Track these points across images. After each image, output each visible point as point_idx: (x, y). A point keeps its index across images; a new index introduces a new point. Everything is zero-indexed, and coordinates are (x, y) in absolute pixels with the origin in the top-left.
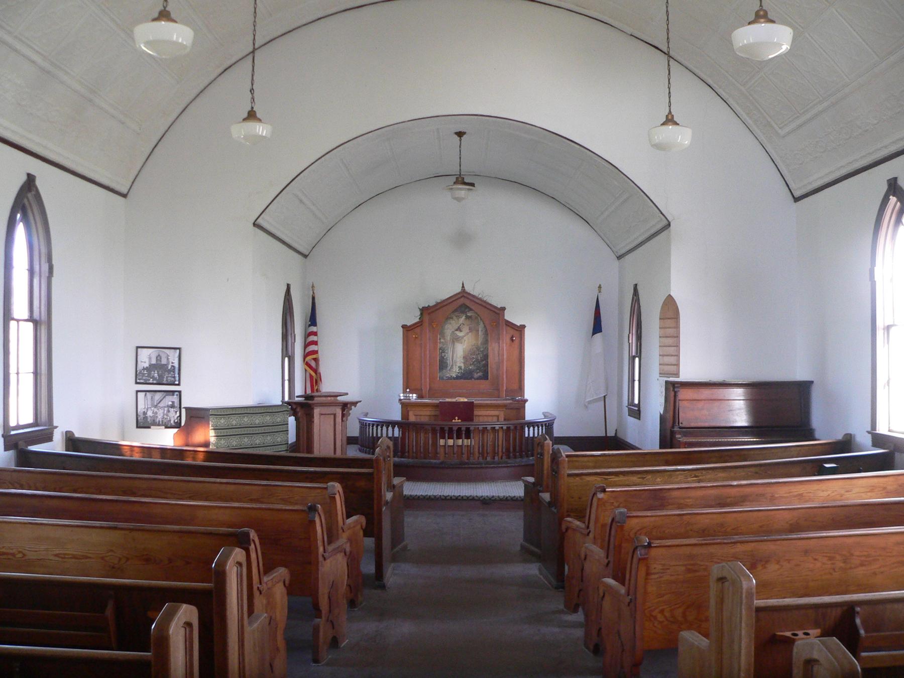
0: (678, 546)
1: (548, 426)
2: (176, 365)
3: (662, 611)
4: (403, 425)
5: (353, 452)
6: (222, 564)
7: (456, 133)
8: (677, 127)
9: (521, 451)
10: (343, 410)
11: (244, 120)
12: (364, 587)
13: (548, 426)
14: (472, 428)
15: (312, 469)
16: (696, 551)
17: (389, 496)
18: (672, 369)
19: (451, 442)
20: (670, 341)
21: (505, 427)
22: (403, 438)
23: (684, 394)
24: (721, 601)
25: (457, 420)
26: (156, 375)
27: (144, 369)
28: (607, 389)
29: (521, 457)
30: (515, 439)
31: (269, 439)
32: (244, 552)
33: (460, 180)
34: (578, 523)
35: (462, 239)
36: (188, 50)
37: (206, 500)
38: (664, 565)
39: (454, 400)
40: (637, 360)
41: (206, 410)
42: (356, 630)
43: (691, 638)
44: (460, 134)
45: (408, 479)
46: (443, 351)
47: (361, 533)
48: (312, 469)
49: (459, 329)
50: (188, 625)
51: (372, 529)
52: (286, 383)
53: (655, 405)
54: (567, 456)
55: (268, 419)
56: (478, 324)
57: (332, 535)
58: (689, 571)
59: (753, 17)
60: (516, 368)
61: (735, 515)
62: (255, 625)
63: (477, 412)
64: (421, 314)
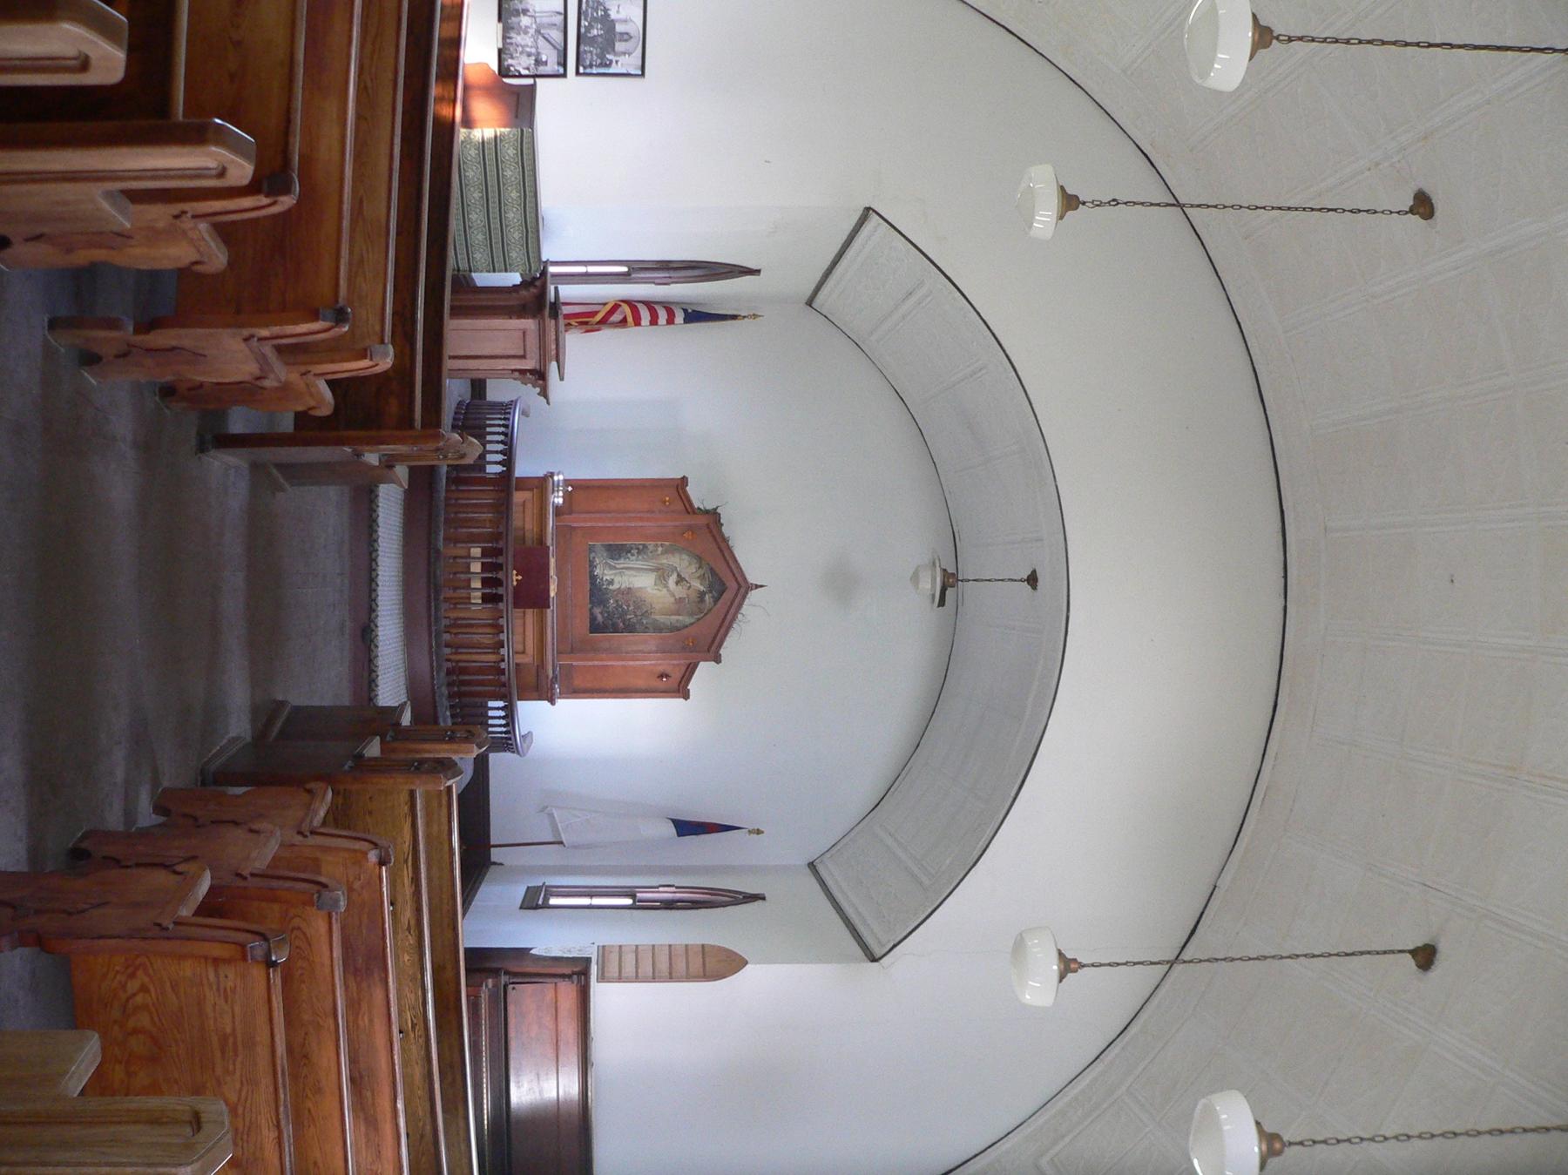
0: (271, 1020)
1: (507, 743)
2: (611, 71)
3: (144, 989)
4: (506, 481)
5: (455, 391)
6: (221, 137)
7: (1034, 572)
8: (1056, 977)
9: (460, 695)
10: (532, 372)
11: (1062, 188)
12: (206, 415)
13: (507, 743)
14: (501, 606)
15: (420, 315)
16: (262, 1052)
17: (372, 458)
18: (613, 969)
19: (476, 567)
20: (663, 966)
21: (503, 665)
22: (485, 481)
23: (568, 991)
24: (155, 1120)
25: (515, 578)
26: (595, 32)
27: (606, 10)
28: (575, 847)
29: (451, 696)
30: (482, 683)
31: (478, 237)
32: (246, 182)
33: (950, 580)
34: (322, 813)
35: (842, 583)
36: (1198, 80)
37: (359, 117)
38: (234, 990)
39: (552, 572)
40: (628, 901)
41: (531, 124)
42: (117, 399)
43: (85, 1058)
44: (1032, 580)
45: (405, 492)
46: (642, 550)
47: (300, 408)
48: (420, 315)
49: (680, 580)
50: (84, 65)
51: (309, 428)
52: (581, 269)
53: (549, 938)
54: (449, 789)
55: (515, 235)
56: (692, 614)
57: (294, 352)
58: (224, 1039)
59: (1268, 1128)
60: (612, 683)
61: (337, 1114)
62: (106, 205)
63: (530, 614)
64: (707, 512)
